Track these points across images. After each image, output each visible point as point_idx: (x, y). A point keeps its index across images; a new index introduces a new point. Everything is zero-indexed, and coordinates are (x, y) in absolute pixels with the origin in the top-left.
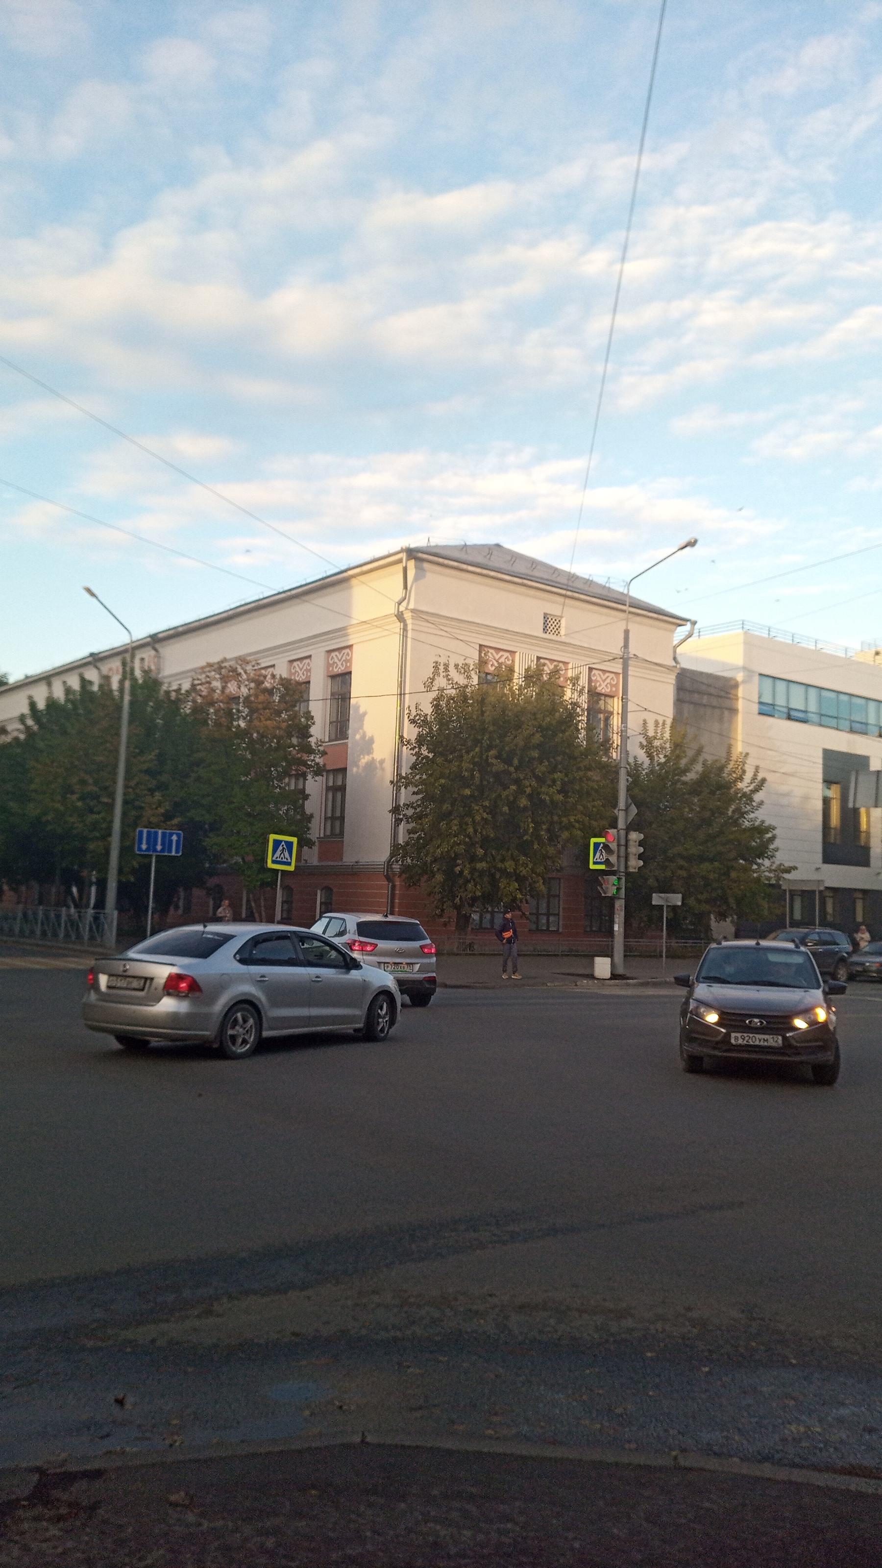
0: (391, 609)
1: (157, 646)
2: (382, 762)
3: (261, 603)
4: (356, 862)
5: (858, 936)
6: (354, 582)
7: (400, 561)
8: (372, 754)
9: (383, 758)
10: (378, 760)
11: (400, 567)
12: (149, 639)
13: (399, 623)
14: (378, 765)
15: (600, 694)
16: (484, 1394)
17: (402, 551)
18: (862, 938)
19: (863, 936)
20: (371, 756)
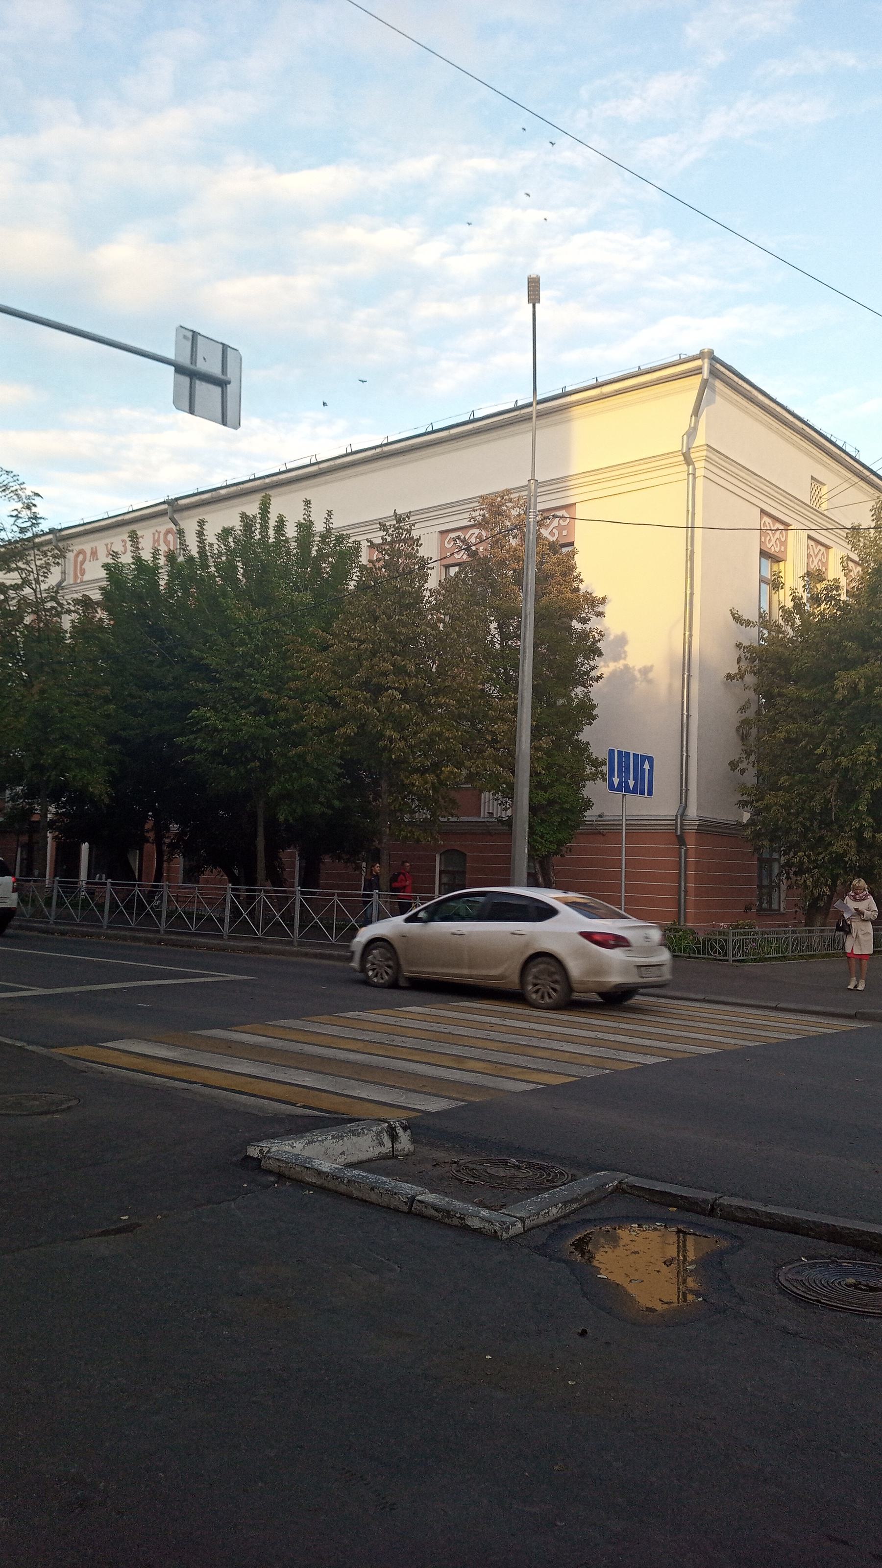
0: (676, 444)
1: (176, 516)
2: (646, 671)
3: (386, 449)
4: (600, 816)
5: (11, 802)
6: (577, 411)
7: (698, 371)
8: (625, 659)
9: (649, 664)
10: (637, 668)
11: (696, 381)
12: (165, 506)
13: (685, 466)
14: (638, 675)
15: (807, 571)
16: (512, 1508)
17: (701, 356)
18: (859, 912)
19: (862, 906)
20: (622, 662)
